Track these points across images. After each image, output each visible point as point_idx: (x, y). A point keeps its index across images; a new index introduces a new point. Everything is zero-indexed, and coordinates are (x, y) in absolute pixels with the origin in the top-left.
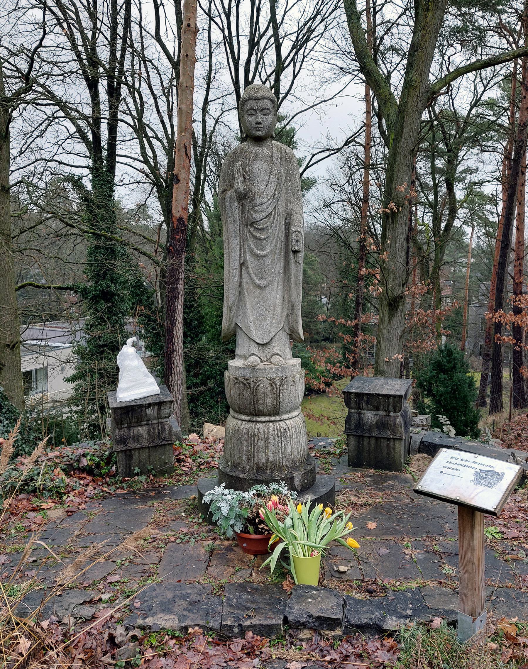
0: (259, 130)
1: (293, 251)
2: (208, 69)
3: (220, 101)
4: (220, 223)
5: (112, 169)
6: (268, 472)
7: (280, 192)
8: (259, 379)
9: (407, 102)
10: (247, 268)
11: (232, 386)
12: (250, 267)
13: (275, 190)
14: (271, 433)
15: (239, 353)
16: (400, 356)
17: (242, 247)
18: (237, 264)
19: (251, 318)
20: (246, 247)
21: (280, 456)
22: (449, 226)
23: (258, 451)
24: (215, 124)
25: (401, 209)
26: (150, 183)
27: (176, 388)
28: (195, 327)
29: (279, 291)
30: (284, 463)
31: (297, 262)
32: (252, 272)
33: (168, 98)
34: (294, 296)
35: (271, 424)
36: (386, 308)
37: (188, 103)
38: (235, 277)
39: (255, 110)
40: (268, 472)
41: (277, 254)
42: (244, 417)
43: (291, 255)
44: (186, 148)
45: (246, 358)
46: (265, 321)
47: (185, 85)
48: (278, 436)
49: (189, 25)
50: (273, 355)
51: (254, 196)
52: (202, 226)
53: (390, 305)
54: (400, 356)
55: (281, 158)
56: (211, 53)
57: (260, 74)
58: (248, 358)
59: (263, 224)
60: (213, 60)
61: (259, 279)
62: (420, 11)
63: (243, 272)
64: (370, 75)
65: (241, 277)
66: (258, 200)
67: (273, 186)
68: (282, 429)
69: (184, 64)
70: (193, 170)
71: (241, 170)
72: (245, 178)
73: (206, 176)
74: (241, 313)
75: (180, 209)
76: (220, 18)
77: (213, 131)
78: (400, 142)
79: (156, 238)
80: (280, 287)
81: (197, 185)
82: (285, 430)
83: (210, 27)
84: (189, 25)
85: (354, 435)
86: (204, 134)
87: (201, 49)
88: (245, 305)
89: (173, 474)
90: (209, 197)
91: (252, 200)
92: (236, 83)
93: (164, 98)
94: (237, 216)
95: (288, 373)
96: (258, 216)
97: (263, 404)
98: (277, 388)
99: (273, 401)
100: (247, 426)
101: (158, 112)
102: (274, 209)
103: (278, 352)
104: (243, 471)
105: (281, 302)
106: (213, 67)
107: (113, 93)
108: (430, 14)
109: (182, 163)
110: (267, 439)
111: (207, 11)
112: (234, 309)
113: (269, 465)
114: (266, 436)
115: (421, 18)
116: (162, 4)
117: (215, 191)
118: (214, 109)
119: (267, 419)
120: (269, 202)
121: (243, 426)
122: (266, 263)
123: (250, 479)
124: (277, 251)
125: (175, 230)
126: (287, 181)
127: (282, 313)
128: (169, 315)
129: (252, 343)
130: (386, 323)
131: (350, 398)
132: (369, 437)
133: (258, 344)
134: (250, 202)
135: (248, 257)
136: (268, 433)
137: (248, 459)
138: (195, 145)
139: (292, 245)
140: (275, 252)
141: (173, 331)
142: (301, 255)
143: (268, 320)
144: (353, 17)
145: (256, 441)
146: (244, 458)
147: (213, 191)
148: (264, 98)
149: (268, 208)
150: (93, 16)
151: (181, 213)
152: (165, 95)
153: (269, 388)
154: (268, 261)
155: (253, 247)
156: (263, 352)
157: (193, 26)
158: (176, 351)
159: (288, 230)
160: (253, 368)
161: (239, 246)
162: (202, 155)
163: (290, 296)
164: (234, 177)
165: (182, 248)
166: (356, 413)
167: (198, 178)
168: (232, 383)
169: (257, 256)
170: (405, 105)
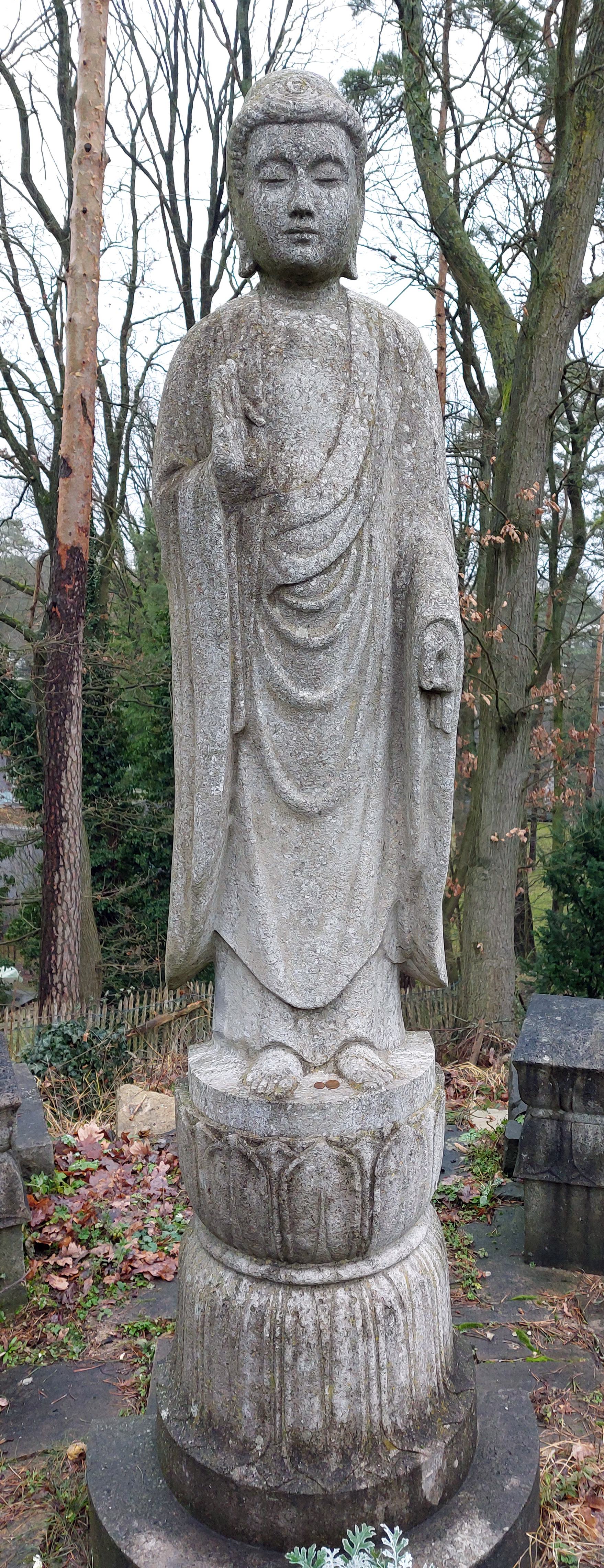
0: (305, 242)
1: (422, 690)
2: (131, 262)
3: (155, 323)
4: (156, 555)
6: (333, 1461)
7: (377, 478)
8: (300, 1144)
9: (539, 318)
10: (258, 747)
11: (204, 1158)
12: (268, 744)
13: (362, 470)
14: (342, 1326)
15: (225, 1030)
16: (522, 832)
17: (240, 674)
18: (223, 736)
19: (272, 920)
20: (256, 677)
21: (375, 1400)
22: (573, 565)
23: (296, 1389)
24: (146, 369)
25: (526, 536)
26: (21, 478)
27: (67, 897)
28: (109, 755)
29: (371, 828)
30: (387, 1422)
31: (436, 728)
32: (276, 764)
33: (52, 314)
34: (422, 844)
35: (341, 1294)
36: (494, 735)
37: (87, 310)
38: (214, 781)
40: (333, 1461)
41: (365, 699)
42: (243, 1264)
43: (418, 706)
44: (83, 403)
45: (250, 1052)
46: (319, 929)
47: (80, 271)
48: (366, 1335)
49: (88, 149)
50: (346, 1044)
51: (286, 488)
52: (122, 559)
53: (502, 729)
54: (522, 832)
55: (383, 352)
56: (136, 231)
57: (230, 275)
58: (257, 1053)
59: (318, 593)
60: (140, 246)
61: (301, 788)
62: (568, 128)
63: (245, 761)
64: (462, 264)
65: (235, 778)
66: (300, 505)
67: (352, 455)
68: (379, 1308)
69: (78, 229)
70: (101, 450)
71: (236, 392)
72: (250, 423)
73: (129, 466)
74: (234, 901)
75: (73, 529)
76: (155, 163)
77: (141, 383)
78: (524, 399)
79: (32, 583)
80: (375, 814)
81: (112, 483)
82: (390, 1310)
83: (133, 181)
84: (88, 149)
85: (542, 1182)
86: (125, 386)
88: (250, 874)
89: (22, 1309)
90: (135, 505)
91: (279, 502)
92: (185, 289)
93: (45, 315)
94: (220, 564)
95: (401, 1112)
96: (300, 565)
97: (314, 1230)
98: (363, 1177)
99: (348, 1218)
100: (256, 1300)
101: (35, 339)
102: (358, 538)
103: (361, 1032)
104: (244, 1453)
105: (375, 862)
109: (77, 434)
110: (327, 1354)
111: (128, 149)
112: (210, 891)
113: (335, 1438)
114: (326, 1338)
117: (148, 496)
119: (327, 1274)
120: (341, 512)
121: (241, 1298)
122: (327, 732)
123: (270, 1491)
124: (368, 691)
125: (62, 571)
126: (400, 439)
127: (378, 898)
128: (52, 747)
129: (273, 1004)
130: (493, 764)
131: (535, 1080)
132: (588, 1189)
133: (293, 1008)
134: (271, 511)
135: (263, 709)
136: (333, 1328)
137: (262, 1414)
138: (108, 405)
139: (421, 671)
140: (358, 695)
141: (60, 779)
142: (451, 707)
143: (332, 925)
144: (426, 143)
145: (288, 1358)
146: (247, 1409)
147: (143, 495)
148: (323, 117)
149: (335, 534)
151: (75, 537)
152: (47, 309)
153: (336, 1176)
154: (335, 725)
155: (282, 675)
156: (312, 1033)
157: (96, 149)
158: (67, 821)
159: (404, 613)
160: (279, 1103)
161: (227, 673)
162: (120, 425)
163: (408, 842)
164: (208, 419)
165: (78, 609)
166: (551, 1118)
167: (113, 469)
168: (201, 1144)
169: (295, 709)
170: (536, 324)
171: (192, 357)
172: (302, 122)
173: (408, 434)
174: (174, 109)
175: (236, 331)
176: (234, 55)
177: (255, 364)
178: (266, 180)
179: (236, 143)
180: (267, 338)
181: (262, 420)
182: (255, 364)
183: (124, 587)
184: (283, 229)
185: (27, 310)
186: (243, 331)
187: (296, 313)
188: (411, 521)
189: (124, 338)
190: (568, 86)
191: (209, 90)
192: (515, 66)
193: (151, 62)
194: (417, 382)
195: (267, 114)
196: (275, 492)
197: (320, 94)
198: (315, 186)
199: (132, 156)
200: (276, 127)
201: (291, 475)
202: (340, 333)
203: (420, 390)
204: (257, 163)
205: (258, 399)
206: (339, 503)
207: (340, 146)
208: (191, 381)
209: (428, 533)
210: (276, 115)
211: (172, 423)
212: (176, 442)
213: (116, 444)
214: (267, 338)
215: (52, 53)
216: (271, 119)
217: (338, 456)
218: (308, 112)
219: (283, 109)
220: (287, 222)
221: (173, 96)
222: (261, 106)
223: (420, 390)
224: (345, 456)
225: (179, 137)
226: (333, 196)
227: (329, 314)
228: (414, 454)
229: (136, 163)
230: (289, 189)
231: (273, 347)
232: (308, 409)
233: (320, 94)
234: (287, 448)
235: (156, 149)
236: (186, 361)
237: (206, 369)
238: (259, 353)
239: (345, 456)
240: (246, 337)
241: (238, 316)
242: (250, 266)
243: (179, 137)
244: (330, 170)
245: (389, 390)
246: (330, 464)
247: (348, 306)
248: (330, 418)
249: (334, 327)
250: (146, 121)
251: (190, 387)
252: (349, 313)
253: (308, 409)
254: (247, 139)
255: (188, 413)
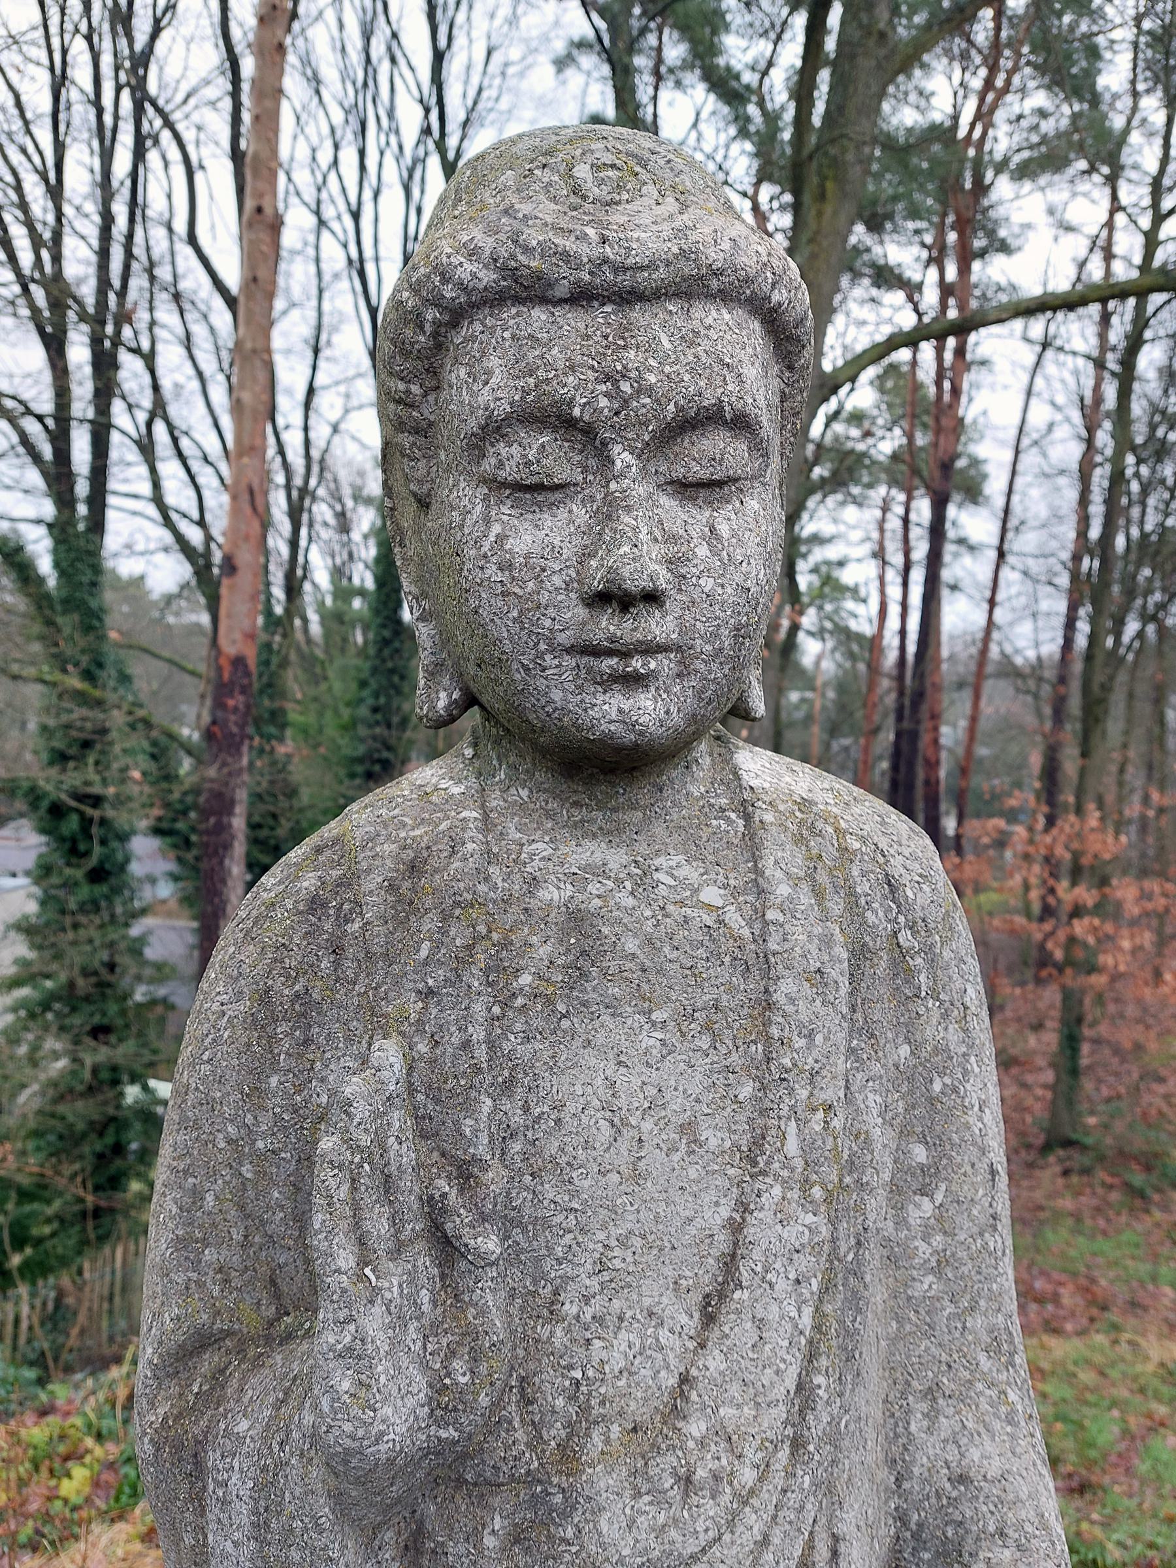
0: (633, 681)
3: (342, 389)
5: (97, 524)
39: (583, 434)
44: (251, 492)
49: (259, 210)
51: (568, 1457)
52: (306, 630)
55: (860, 954)
56: (321, 291)
60: (326, 306)
75: (238, 636)
84: (259, 210)
87: (296, 275)
106: (326, 320)
107: (104, 364)
108: (828, 209)
115: (810, 214)
116: (202, 167)
118: (328, 405)
148: (696, 284)
150: (55, 192)
157: (268, 210)
165: (242, 727)
171: (264, 997)
172: (628, 298)
173: (922, 1167)
174: (363, 168)
175: (403, 923)
176: (427, 111)
177: (466, 1045)
178: (504, 485)
179: (406, 354)
180: (506, 945)
181: (491, 1244)
182: (466, 1045)
183: (309, 662)
184: (562, 638)
185: (200, 375)
186: (430, 923)
187: (592, 852)
188: (932, 1416)
189: (307, 405)
190: (806, 152)
191: (401, 147)
192: (733, 131)
193: (338, 116)
194: (946, 1015)
195: (510, 272)
196: (531, 1478)
197: (684, 207)
198: (667, 502)
199: (317, 213)
200: (539, 314)
201: (585, 1409)
202: (733, 917)
203: (953, 1035)
204: (473, 425)
205: (475, 1160)
206: (745, 1499)
207: (751, 372)
208: (258, 1075)
209: (986, 1456)
210: (539, 276)
211: (197, 1195)
212: (209, 1255)
213: (295, 513)
214: (506, 945)
215: (227, 104)
216: (523, 288)
217: (742, 1333)
218: (651, 266)
219: (565, 256)
220: (570, 617)
221: (362, 153)
222: (487, 243)
223: (953, 1035)
224: (760, 1324)
225: (368, 195)
226: (724, 529)
227: (694, 851)
228: (942, 1222)
229: (322, 223)
230: (581, 514)
231: (526, 979)
232: (638, 1177)
233: (684, 207)
234: (570, 1309)
235: (342, 207)
236: (244, 1006)
237: (307, 1042)
238: (478, 1007)
239: (760, 1324)
240: (437, 946)
241: (414, 868)
242: (452, 703)
243: (368, 195)
244: (720, 450)
245: (877, 1069)
246: (714, 1362)
247: (747, 818)
248: (708, 1197)
249: (712, 895)
250: (332, 177)
251: (256, 1094)
252: (752, 844)
253: (638, 1177)
254: (439, 347)
255: (247, 1171)
